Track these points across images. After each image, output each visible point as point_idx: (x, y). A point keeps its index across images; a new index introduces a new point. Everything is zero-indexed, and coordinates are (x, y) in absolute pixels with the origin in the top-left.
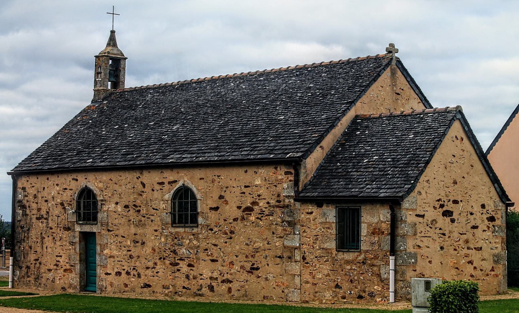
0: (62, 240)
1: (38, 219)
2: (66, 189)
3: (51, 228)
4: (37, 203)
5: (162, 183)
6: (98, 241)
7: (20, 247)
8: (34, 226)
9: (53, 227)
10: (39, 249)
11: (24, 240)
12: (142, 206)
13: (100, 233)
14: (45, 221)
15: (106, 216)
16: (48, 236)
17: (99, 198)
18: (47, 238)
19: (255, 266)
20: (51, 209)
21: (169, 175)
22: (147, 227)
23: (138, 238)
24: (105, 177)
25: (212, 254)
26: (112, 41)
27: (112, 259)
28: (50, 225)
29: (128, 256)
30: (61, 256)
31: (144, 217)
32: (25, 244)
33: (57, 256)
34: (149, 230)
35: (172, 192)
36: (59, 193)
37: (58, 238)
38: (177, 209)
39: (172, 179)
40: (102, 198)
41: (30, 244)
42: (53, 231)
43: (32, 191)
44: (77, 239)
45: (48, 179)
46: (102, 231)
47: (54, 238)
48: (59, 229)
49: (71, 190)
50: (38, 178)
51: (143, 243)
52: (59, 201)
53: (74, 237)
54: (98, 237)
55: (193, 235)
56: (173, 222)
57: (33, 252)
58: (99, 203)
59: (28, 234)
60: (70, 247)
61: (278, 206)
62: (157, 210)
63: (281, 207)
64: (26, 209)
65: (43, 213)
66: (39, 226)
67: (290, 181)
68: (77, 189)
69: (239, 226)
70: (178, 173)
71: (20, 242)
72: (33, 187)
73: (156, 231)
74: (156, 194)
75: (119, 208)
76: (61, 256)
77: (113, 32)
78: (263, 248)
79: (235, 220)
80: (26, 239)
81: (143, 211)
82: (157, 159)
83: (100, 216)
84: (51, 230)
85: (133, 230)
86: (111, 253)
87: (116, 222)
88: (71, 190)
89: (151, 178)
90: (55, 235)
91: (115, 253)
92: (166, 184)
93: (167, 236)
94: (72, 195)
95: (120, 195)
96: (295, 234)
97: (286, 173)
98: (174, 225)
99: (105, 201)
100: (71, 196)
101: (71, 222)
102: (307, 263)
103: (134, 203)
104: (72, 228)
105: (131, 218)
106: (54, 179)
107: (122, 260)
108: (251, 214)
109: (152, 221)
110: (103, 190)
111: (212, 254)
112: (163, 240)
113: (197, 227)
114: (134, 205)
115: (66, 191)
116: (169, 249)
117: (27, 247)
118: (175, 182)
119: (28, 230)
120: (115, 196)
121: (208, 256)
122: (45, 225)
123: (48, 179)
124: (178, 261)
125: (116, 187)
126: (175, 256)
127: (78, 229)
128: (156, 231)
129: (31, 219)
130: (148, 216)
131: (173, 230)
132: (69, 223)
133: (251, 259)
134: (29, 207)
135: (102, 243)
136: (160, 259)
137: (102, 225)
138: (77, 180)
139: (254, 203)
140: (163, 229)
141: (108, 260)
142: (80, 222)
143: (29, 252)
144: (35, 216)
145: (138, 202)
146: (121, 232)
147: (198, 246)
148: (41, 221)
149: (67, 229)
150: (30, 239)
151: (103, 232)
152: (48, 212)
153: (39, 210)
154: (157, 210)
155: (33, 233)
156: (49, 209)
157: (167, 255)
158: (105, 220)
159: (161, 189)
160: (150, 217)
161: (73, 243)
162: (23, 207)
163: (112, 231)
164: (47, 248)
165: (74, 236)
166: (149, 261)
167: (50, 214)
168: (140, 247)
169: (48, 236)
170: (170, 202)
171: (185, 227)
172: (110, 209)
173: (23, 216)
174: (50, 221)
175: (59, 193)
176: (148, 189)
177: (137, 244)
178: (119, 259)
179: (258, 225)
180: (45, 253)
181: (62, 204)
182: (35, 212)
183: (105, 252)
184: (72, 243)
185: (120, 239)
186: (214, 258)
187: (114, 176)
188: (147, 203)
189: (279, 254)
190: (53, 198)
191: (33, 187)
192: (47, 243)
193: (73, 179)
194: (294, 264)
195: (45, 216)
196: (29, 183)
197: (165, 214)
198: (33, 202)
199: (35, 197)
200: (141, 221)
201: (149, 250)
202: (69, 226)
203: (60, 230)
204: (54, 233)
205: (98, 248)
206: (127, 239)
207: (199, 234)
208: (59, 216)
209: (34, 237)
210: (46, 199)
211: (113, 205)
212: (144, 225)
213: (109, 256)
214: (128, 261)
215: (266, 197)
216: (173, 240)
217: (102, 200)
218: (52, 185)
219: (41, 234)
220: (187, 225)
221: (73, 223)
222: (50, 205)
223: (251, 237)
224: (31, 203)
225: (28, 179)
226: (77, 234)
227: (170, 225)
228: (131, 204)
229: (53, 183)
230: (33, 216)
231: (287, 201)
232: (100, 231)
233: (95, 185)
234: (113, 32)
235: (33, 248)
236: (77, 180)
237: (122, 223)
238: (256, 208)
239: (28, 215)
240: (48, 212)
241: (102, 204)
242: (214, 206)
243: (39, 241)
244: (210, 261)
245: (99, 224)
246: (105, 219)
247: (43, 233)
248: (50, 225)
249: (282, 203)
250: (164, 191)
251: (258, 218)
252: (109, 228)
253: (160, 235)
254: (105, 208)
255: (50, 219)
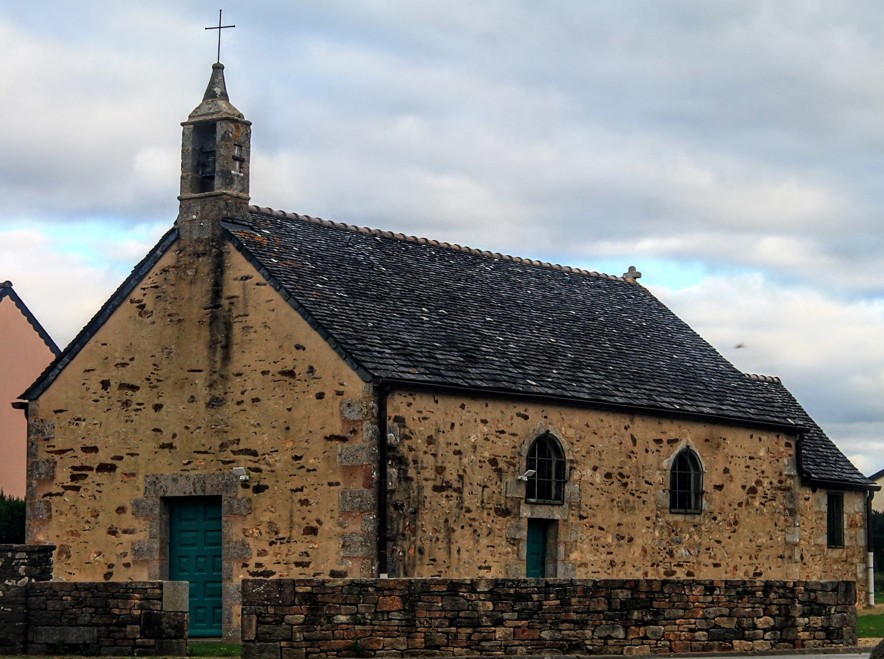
0: (492, 535)
1: (436, 489)
2: (503, 432)
3: (469, 511)
4: (435, 455)
5: (658, 441)
6: (562, 537)
7: (393, 551)
8: (427, 505)
9: (473, 508)
10: (441, 555)
11: (403, 535)
12: (632, 477)
13: (566, 521)
14: (455, 494)
15: (577, 490)
16: (463, 527)
17: (569, 457)
18: (459, 531)
19: (758, 571)
20: (468, 470)
21: (671, 429)
22: (637, 512)
23: (623, 530)
24: (578, 418)
25: (715, 555)
26: (216, 89)
27: (582, 569)
28: (466, 504)
29: (608, 562)
30: (489, 568)
31: (633, 495)
32: (406, 545)
33: (480, 568)
34: (639, 518)
35: (673, 457)
36: (487, 439)
37: (485, 532)
38: (554, 485)
39: (673, 435)
40: (571, 458)
41: (419, 543)
42: (472, 515)
43: (423, 429)
44: (524, 534)
45: (463, 407)
46: (571, 517)
47: (475, 531)
48: (485, 512)
49: (514, 435)
50: (487, 406)
51: (631, 540)
52: (487, 454)
53: (519, 529)
54: (562, 529)
55: (695, 526)
56: (673, 506)
57: (426, 560)
58: (568, 466)
59: (413, 521)
60: (509, 550)
61: (780, 489)
62: (650, 484)
63: (783, 490)
64: (407, 465)
65: (451, 475)
66: (437, 507)
67: (790, 455)
68: (527, 436)
69: (743, 513)
70: (679, 427)
71: (394, 540)
72: (425, 418)
73: (648, 519)
74: (651, 458)
75: (598, 478)
76: (489, 568)
77: (218, 69)
78: (765, 545)
79: (740, 505)
80: (407, 532)
81: (632, 486)
82: (665, 402)
83: (568, 489)
84: (467, 515)
85: (617, 517)
86: (582, 558)
87: (593, 501)
88: (514, 435)
89: (645, 430)
90: (476, 524)
91: (589, 557)
92: (665, 443)
93: (662, 527)
94: (517, 445)
95: (600, 454)
96: (795, 526)
97: (788, 445)
98: (673, 510)
99: (577, 462)
100: (514, 447)
101: (512, 499)
102: (805, 564)
103: (620, 470)
104: (515, 511)
105: (615, 496)
106: (476, 409)
107: (599, 570)
108: (755, 498)
109: (644, 502)
110: (574, 442)
111: (715, 555)
112: (657, 534)
113: (700, 514)
114: (621, 474)
115: (502, 435)
116: (665, 549)
117: (412, 552)
118: (676, 441)
119: (415, 512)
120: (592, 454)
121: (710, 557)
122: (454, 502)
123: (463, 407)
124: (675, 569)
125: (594, 440)
126: (670, 560)
127: (526, 512)
128: (648, 519)
129: (420, 489)
130: (638, 494)
131: (671, 518)
132: (509, 501)
133: (754, 561)
134: (415, 462)
135: (568, 540)
136: (653, 565)
137: (570, 506)
138: (526, 418)
139: (759, 483)
140: (657, 516)
141: (577, 569)
142: (532, 500)
143: (418, 562)
144: (430, 484)
145: (626, 470)
146: (599, 521)
147: (700, 544)
148: (445, 494)
149: (504, 512)
150: (419, 532)
151: (572, 519)
152: (461, 477)
153: (440, 470)
154: (650, 484)
155: (427, 521)
156: (464, 471)
157: (661, 559)
158: (575, 499)
159: (657, 451)
160: (642, 495)
161: (514, 539)
162: (401, 461)
163: (585, 518)
164: (459, 551)
165: (517, 527)
166: (637, 570)
167: (466, 479)
168: (626, 547)
169: (463, 527)
170: (669, 472)
171: (686, 514)
172: (584, 478)
173: (400, 481)
174: (466, 495)
175: (487, 439)
176: (639, 449)
177: (622, 541)
178: (594, 569)
179: (762, 514)
180: (454, 562)
181: (493, 462)
182: (430, 473)
183: (574, 556)
184: (513, 541)
185: (597, 532)
186: (717, 561)
187: (593, 418)
188: (638, 472)
189: (781, 553)
190: (475, 447)
191: (425, 418)
192: (461, 540)
193: (519, 415)
194: (794, 565)
195: (456, 485)
196: (412, 410)
197: (661, 491)
198: (425, 453)
199: (430, 440)
200: (628, 501)
201: (636, 551)
202: (508, 506)
203: (489, 514)
204: (474, 520)
205: (562, 548)
206: (608, 532)
207: (701, 525)
208: (485, 486)
209: (429, 529)
210: (457, 448)
211: (589, 472)
212: (633, 508)
213: (579, 563)
214: (609, 571)
215: (769, 475)
216: (669, 535)
217: (572, 461)
218: (472, 421)
219: (446, 521)
220: (689, 511)
221: (517, 501)
222: (465, 461)
223: (756, 529)
224: (421, 454)
225: (410, 399)
226: (524, 523)
227: (667, 511)
228: (615, 472)
229: (475, 416)
230: (425, 483)
231: (788, 481)
232: (566, 518)
233: (560, 430)
234: (218, 69)
235: (426, 553)
236: (526, 418)
237: (601, 504)
238: (760, 489)
239: (411, 479)
240: (461, 477)
241: (571, 468)
242: (719, 483)
243: (441, 537)
244: (712, 566)
245: (566, 505)
246: (576, 495)
247: (451, 521)
248: (466, 504)
249: (783, 484)
250: (661, 454)
251: (761, 503)
252: (582, 513)
253: (652, 526)
254: (576, 476)
255: (466, 490)
